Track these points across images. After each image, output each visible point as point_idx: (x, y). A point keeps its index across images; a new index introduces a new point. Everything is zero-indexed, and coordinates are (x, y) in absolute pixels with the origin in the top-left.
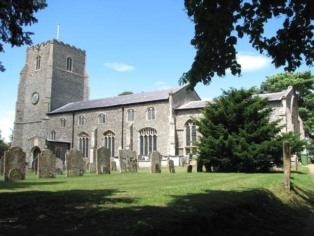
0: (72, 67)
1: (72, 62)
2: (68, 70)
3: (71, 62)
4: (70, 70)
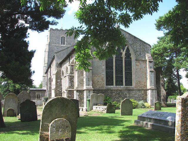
0: (65, 43)
1: (65, 39)
2: (62, 44)
3: (64, 39)
4: (64, 44)
